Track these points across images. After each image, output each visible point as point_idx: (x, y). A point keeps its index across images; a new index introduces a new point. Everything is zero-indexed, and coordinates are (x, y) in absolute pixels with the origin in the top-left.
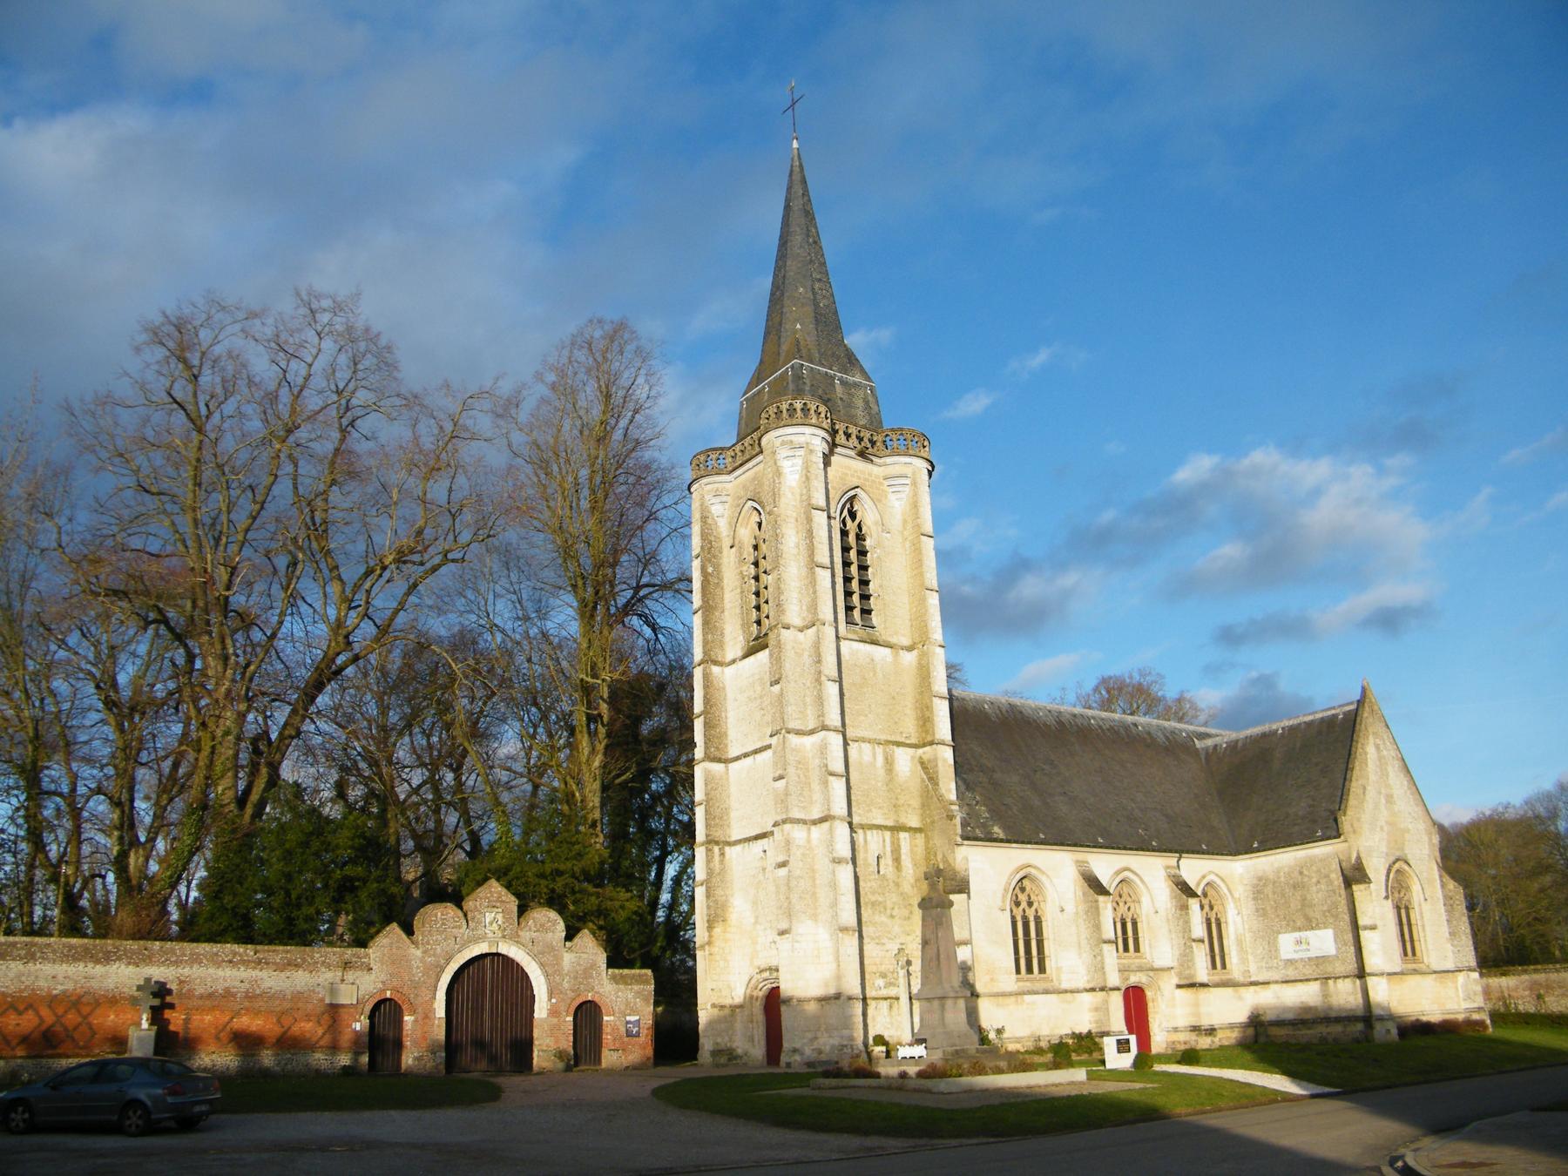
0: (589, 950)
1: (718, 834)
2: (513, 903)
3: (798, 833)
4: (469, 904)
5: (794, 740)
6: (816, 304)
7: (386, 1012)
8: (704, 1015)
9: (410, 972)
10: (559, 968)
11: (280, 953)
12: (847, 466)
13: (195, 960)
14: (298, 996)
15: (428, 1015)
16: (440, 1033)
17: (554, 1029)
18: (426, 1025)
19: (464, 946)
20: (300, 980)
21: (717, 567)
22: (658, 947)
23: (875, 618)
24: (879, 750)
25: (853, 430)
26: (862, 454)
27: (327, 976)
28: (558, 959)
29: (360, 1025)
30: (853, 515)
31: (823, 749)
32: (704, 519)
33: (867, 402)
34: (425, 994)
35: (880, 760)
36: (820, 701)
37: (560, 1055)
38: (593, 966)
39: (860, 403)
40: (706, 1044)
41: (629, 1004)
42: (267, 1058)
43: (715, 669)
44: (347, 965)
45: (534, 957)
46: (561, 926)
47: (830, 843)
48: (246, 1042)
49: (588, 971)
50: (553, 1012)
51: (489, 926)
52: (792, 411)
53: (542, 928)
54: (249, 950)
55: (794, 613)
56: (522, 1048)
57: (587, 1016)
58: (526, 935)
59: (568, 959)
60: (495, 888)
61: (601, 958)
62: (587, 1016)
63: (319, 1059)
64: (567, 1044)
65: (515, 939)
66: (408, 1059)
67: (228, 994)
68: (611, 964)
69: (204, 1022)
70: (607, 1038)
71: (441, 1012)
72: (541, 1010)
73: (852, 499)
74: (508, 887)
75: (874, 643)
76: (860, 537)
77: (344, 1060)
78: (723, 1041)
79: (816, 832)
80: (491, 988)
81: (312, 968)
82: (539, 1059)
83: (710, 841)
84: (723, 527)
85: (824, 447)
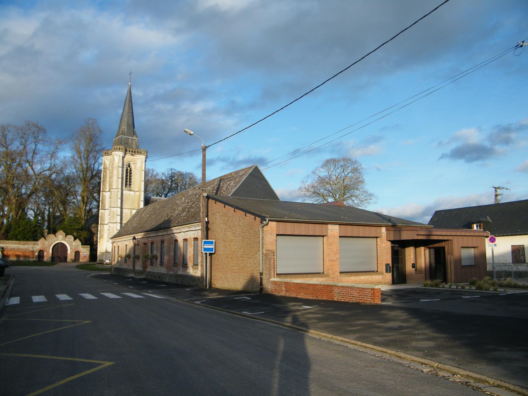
0: (78, 242)
1: (102, 223)
2: (64, 234)
3: (112, 225)
4: (56, 234)
5: (112, 209)
6: (128, 122)
7: (41, 252)
8: (98, 254)
9: (47, 245)
10: (72, 245)
11: (23, 242)
12: (128, 157)
13: (8, 243)
14: (26, 249)
15: (48, 252)
16: (51, 255)
17: (71, 255)
18: (48, 254)
19: (55, 241)
20: (26, 246)
21: (106, 174)
22: (91, 241)
23: (132, 186)
24: (129, 210)
25: (131, 150)
26: (132, 155)
27: (31, 246)
28: (72, 244)
29: (36, 254)
30: (129, 166)
31: (117, 210)
32: (104, 164)
33: (136, 143)
34: (48, 249)
35: (129, 212)
36: (117, 202)
37: (72, 260)
38: (79, 245)
39: (134, 143)
40: (98, 259)
41: (85, 251)
42: (22, 259)
43: (104, 193)
44: (34, 244)
45: (68, 243)
46: (73, 238)
47: (116, 227)
48: (18, 256)
49: (78, 246)
50: (71, 252)
51: (60, 238)
52: (117, 148)
53: (70, 239)
54: (17, 242)
55: (114, 186)
56: (66, 258)
57: (77, 253)
58: (66, 239)
59: (74, 244)
60: (61, 232)
61: (80, 243)
62: (77, 253)
63: (31, 259)
64: (73, 258)
65: (64, 240)
66: (45, 259)
67: (14, 249)
68: (82, 244)
69: (10, 253)
70: (81, 257)
71: (51, 252)
72: (69, 252)
73: (129, 164)
74: (64, 232)
75: (130, 191)
76: (131, 170)
77: (34, 259)
78: (101, 258)
79: (115, 224)
80: (60, 249)
81: (28, 245)
82: (68, 260)
83: (101, 224)
84: (108, 165)
85: (123, 155)
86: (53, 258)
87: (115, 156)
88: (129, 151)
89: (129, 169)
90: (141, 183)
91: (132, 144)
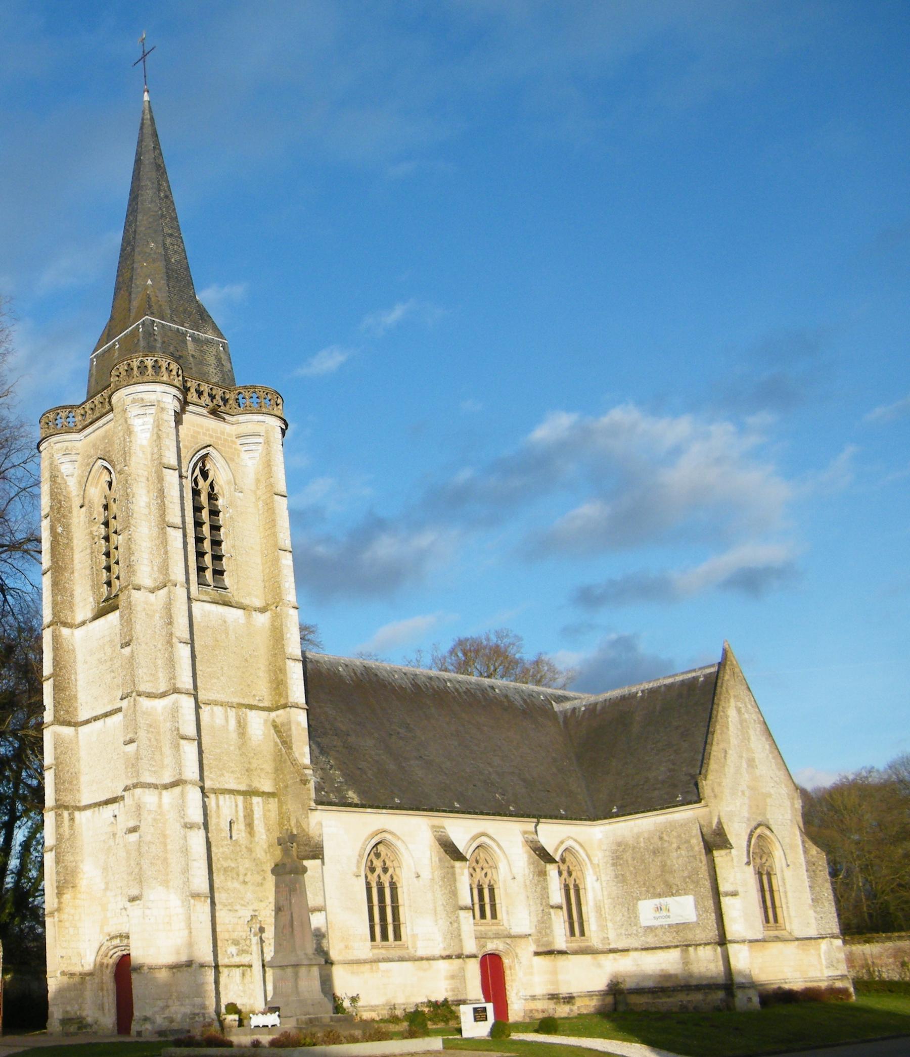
1: (68, 799)
3: (149, 798)
5: (144, 702)
8: (53, 983)
21: (67, 527)
23: (227, 579)
24: (232, 713)
30: (205, 474)
31: (175, 712)
32: (53, 478)
36: (171, 663)
40: (56, 1013)
47: (182, 808)
52: (143, 368)
55: (145, 574)
73: (204, 458)
78: (73, 1010)
79: (168, 797)
83: (60, 806)
84: (72, 486)
86: (236, 1013)
87: (134, 411)
88: (200, 393)
89: (203, 485)
90: (276, 561)
91: (201, 362)
